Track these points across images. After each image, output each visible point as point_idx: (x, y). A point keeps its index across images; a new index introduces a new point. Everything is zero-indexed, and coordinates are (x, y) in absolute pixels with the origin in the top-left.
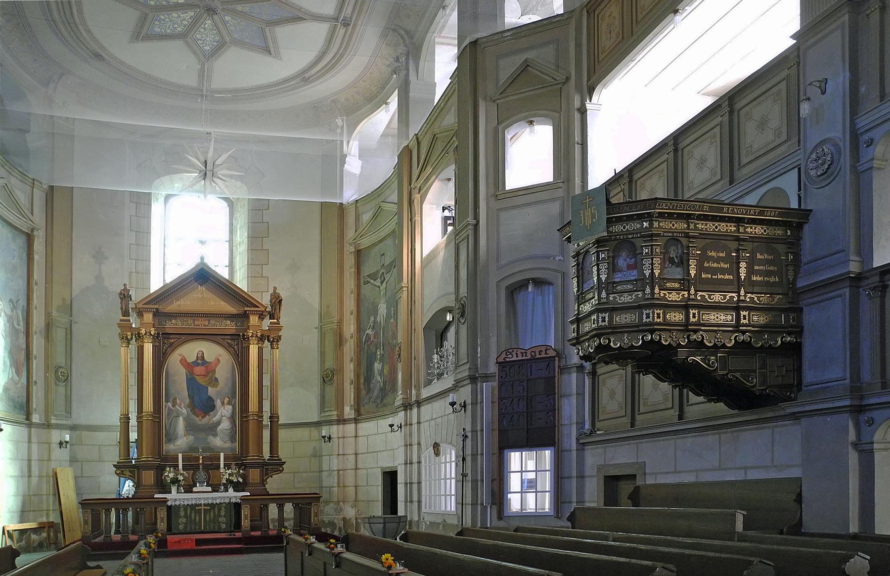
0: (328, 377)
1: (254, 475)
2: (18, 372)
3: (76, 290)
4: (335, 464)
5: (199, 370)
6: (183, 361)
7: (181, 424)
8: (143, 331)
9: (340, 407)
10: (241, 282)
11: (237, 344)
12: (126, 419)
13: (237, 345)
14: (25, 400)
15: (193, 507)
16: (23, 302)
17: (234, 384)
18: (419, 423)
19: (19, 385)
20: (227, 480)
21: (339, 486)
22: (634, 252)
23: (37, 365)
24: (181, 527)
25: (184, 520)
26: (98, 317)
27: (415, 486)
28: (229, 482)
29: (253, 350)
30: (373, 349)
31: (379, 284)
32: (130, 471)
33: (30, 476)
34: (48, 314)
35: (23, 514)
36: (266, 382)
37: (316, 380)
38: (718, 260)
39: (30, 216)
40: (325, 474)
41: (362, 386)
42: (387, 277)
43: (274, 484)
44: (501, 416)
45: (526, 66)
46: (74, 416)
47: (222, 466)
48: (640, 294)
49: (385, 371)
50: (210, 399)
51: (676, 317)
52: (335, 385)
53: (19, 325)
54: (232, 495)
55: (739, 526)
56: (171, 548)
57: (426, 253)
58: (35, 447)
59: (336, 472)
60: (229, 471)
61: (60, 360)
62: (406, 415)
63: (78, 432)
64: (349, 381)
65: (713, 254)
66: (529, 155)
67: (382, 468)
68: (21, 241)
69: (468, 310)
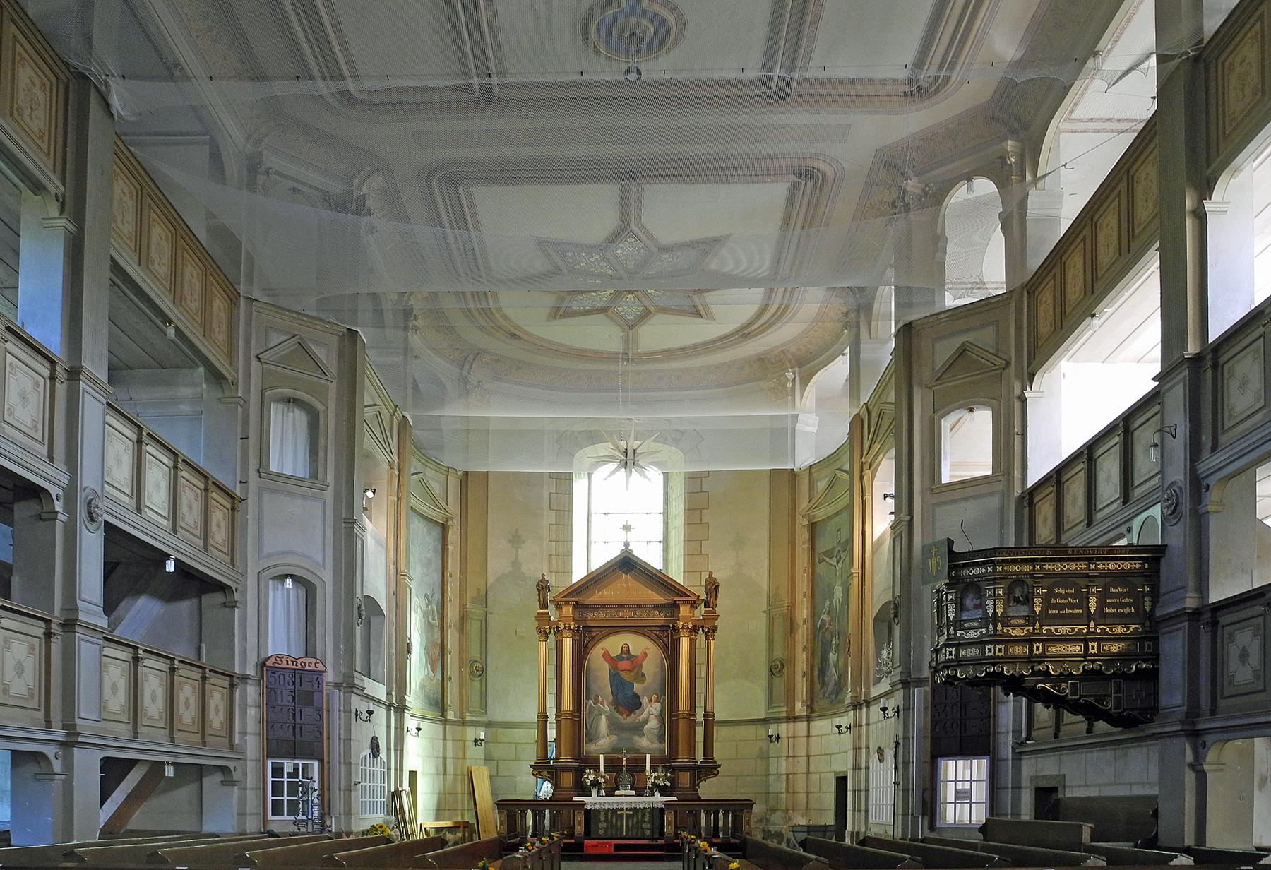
0: (777, 669)
1: (684, 778)
2: (433, 669)
5: (623, 665)
6: (606, 656)
8: (562, 626)
12: (544, 718)
13: (666, 637)
15: (614, 811)
16: (438, 596)
17: (663, 670)
18: (868, 724)
21: (787, 792)
22: (980, 594)
23: (452, 660)
24: (601, 832)
26: (514, 608)
27: (863, 794)
28: (655, 785)
29: (684, 643)
30: (827, 635)
33: (445, 774)
34: (463, 607)
37: (764, 672)
38: (1066, 596)
40: (772, 778)
43: (709, 789)
44: (934, 724)
45: (963, 351)
47: (648, 768)
48: (984, 631)
50: (637, 696)
51: (1021, 650)
54: (658, 799)
55: (1086, 836)
56: (586, 851)
57: (875, 538)
58: (449, 744)
61: (475, 653)
62: (855, 716)
65: (1061, 591)
66: (968, 446)
68: (436, 532)
69: (901, 611)
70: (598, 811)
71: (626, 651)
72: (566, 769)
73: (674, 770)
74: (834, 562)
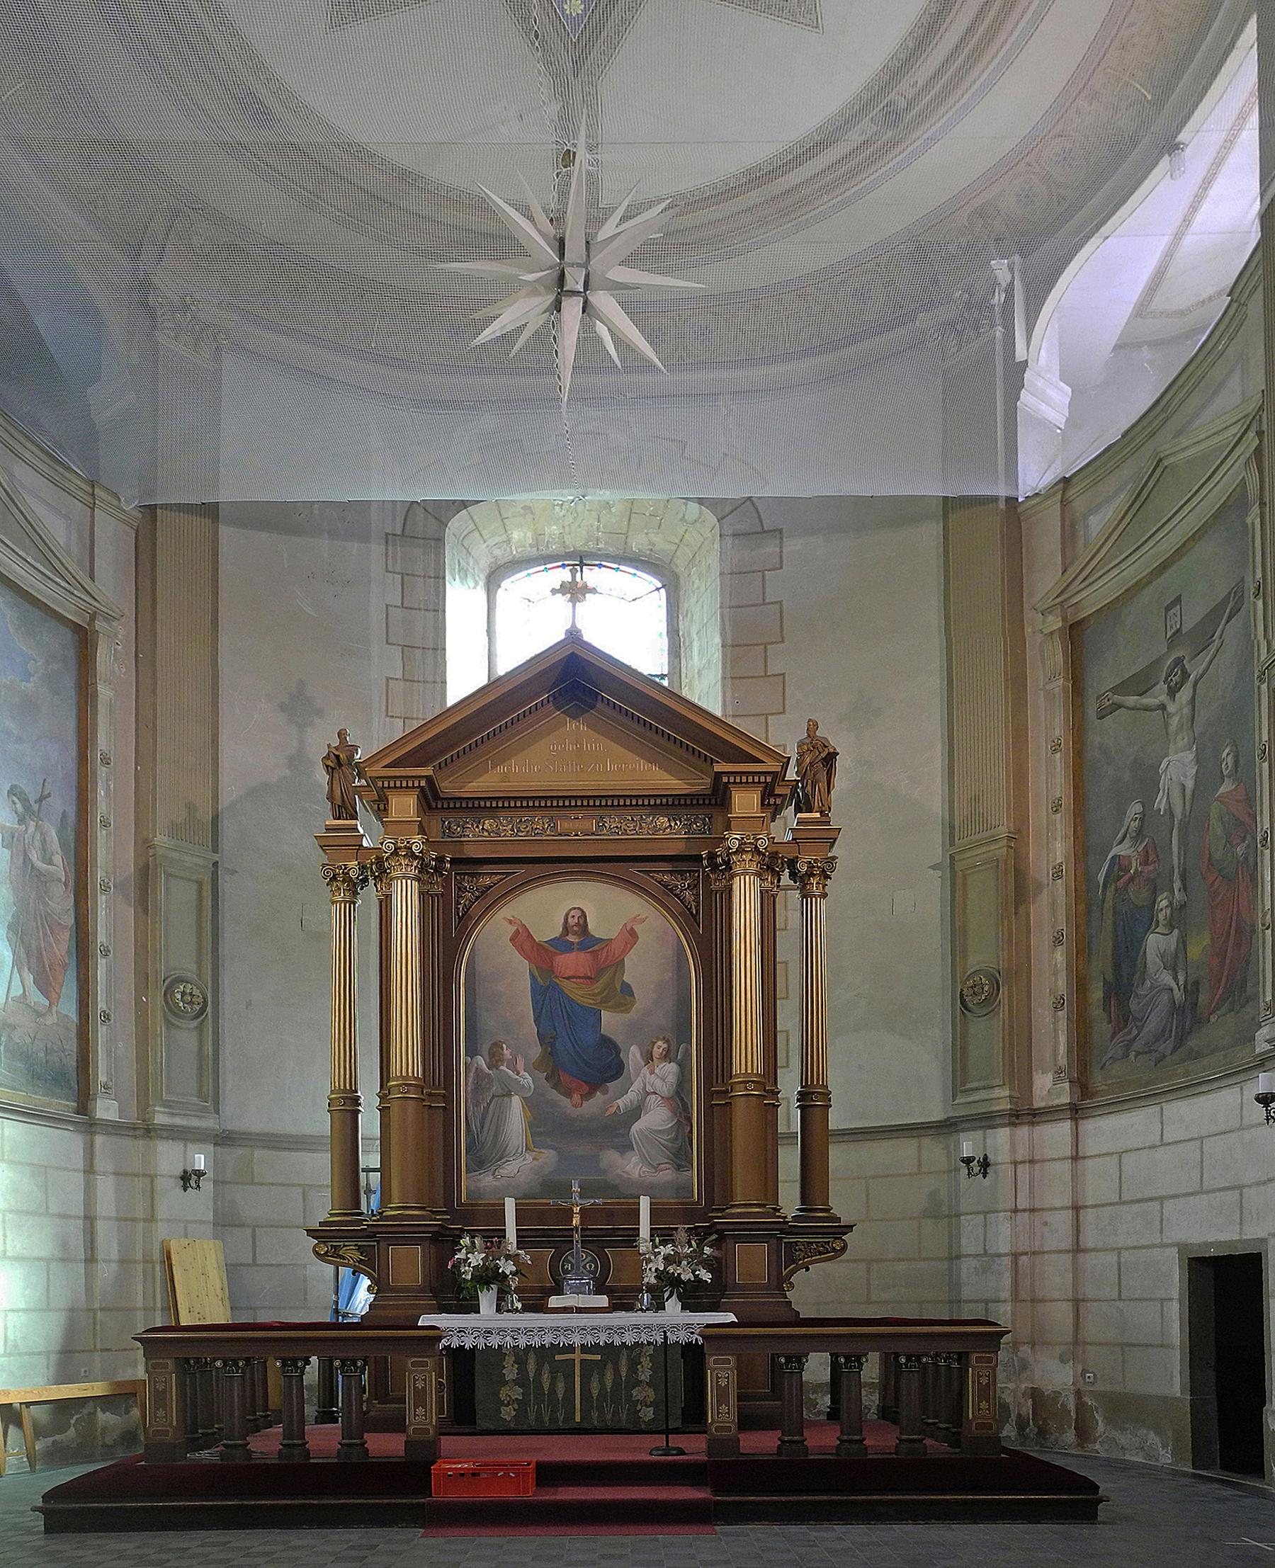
0: (974, 997)
2: (45, 984)
3: (230, 790)
4: (1004, 1236)
5: (569, 962)
6: (522, 939)
7: (516, 1117)
9: (1019, 1071)
10: (706, 690)
13: (692, 885)
14: (72, 1062)
16: (62, 803)
17: (682, 977)
19: (51, 1020)
20: (660, 1275)
21: (1016, 1298)
24: (508, 1413)
25: (517, 1393)
29: (745, 895)
31: (1163, 698)
32: (359, 1248)
33: (91, 1259)
34: (144, 844)
35: (68, 1360)
36: (788, 1019)
37: (936, 1004)
40: (967, 1266)
41: (1096, 1012)
43: (815, 1290)
46: (228, 1108)
49: (1194, 952)
50: (609, 1046)
52: (1003, 1012)
53: (50, 863)
54: (677, 1320)
58: (105, 1187)
59: (1007, 1261)
60: (668, 1250)
61: (180, 956)
63: (240, 1151)
64: (1049, 1002)
67: (1183, 1248)
68: (61, 641)
71: (578, 927)
73: (722, 1237)
74: (1159, 695)
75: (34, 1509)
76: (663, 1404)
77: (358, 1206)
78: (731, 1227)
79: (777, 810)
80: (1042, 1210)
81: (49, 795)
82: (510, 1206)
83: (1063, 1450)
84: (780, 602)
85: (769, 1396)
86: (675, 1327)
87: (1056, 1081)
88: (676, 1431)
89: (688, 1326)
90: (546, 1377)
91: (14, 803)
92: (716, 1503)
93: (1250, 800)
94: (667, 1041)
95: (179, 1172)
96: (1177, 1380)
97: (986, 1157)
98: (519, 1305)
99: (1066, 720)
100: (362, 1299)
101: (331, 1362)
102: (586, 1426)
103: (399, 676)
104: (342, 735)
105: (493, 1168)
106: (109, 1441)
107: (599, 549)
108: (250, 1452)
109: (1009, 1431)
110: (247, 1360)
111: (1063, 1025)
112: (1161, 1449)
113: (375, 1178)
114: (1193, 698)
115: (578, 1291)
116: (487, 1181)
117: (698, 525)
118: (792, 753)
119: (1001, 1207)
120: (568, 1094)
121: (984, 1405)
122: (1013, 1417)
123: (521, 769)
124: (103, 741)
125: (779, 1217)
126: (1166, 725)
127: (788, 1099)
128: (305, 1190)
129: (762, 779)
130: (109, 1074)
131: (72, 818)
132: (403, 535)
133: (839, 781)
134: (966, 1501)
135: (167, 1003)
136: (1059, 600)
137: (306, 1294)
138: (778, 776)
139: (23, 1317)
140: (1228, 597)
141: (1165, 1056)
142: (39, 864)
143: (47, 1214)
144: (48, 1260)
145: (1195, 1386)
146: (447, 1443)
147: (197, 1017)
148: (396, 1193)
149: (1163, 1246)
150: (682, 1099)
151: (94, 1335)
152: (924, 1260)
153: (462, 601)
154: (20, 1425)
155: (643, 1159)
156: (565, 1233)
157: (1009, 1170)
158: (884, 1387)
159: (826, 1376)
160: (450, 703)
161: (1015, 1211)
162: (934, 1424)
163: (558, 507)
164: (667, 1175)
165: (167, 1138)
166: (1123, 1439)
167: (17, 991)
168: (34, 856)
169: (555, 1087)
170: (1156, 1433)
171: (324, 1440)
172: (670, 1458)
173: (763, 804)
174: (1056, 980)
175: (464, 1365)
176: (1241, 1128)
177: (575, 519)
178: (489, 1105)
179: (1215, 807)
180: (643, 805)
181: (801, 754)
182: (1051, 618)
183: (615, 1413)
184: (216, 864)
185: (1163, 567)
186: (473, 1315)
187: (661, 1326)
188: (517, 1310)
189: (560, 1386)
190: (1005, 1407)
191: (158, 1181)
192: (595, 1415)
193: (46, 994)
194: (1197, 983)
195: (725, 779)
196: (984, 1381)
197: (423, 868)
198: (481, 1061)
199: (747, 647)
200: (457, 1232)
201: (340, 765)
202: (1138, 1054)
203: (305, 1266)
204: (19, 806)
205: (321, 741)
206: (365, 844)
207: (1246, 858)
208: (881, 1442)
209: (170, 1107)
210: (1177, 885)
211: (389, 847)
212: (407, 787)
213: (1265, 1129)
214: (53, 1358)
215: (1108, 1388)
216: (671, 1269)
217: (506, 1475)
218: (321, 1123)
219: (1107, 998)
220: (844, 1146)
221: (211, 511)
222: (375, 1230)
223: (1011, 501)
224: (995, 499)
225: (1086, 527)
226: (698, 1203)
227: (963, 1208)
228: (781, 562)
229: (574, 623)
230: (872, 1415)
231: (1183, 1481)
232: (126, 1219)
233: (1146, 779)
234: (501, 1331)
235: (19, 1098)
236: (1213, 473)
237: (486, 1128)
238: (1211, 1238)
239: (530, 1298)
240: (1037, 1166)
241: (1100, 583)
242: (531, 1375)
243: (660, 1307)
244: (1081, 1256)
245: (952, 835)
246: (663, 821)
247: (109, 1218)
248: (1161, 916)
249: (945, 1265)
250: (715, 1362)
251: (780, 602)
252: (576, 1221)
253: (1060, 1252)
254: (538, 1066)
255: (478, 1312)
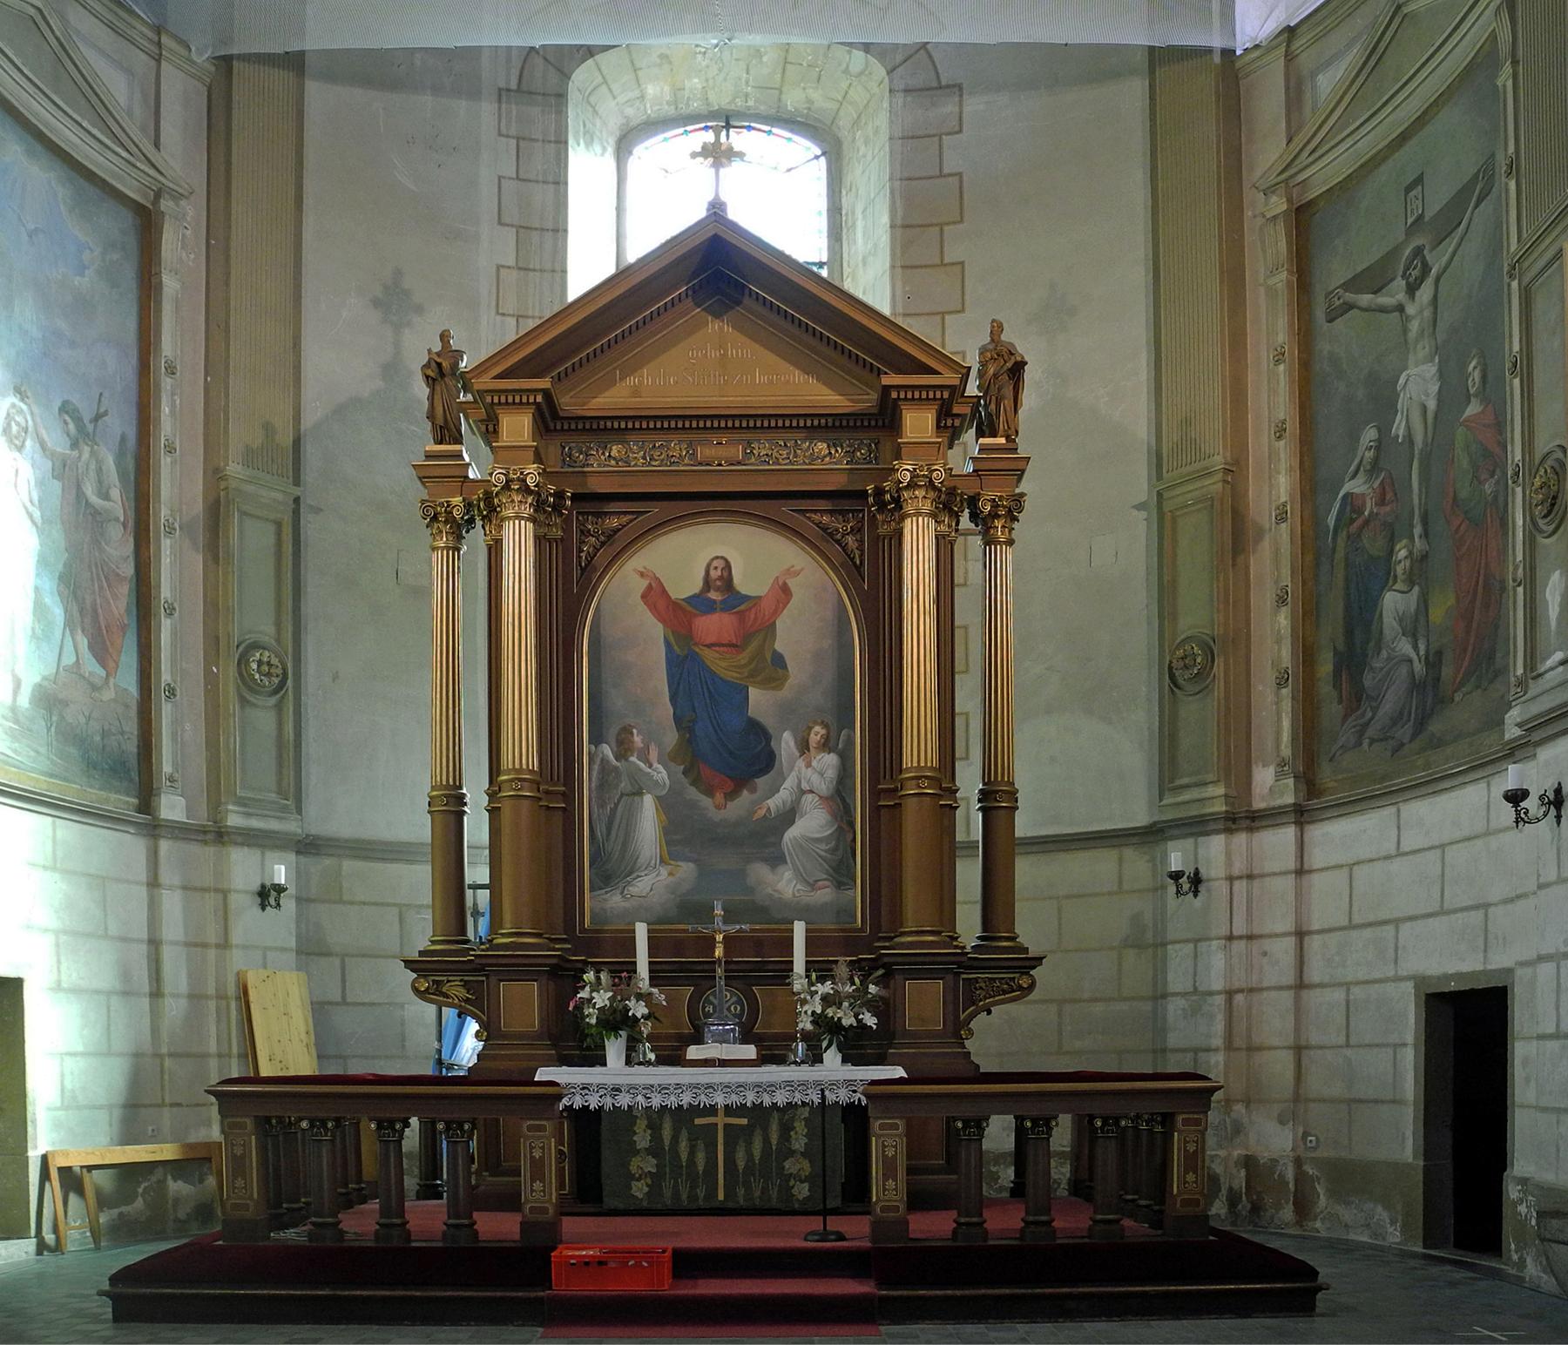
1: (924, 1001)
2: (101, 650)
4: (1217, 969)
5: (713, 626)
6: (655, 595)
9: (1238, 771)
10: (872, 283)
11: (857, 530)
13: (854, 528)
14: (132, 747)
15: (683, 1116)
16: (120, 423)
17: (844, 647)
19: (108, 695)
20: (817, 1019)
21: (1229, 1046)
24: (639, 1189)
25: (650, 1165)
29: (918, 540)
31: (1401, 296)
32: (466, 985)
34: (215, 475)
35: (134, 1115)
36: (968, 700)
39: (148, 148)
40: (1175, 1007)
41: (1325, 689)
42: (1437, 262)
43: (999, 1037)
46: (312, 808)
49: (1437, 614)
50: (758, 733)
52: (1219, 690)
53: (107, 497)
54: (836, 1074)
58: (172, 903)
59: (1220, 1000)
60: (826, 988)
61: (256, 618)
63: (328, 861)
64: (1271, 676)
67: (1420, 981)
68: (118, 224)
70: (626, 1116)
72: (513, 967)
73: (889, 971)
74: (1396, 292)
75: (101, 1293)
76: (820, 1179)
77: (463, 931)
78: (900, 959)
79: (954, 435)
80: (1261, 936)
81: (106, 413)
82: (641, 932)
83: (1279, 1231)
84: (960, 175)
85: (944, 1166)
86: (834, 1084)
87: (1279, 776)
88: (835, 1212)
89: (849, 1083)
90: (683, 1146)
91: (66, 423)
92: (882, 1299)
93: (1500, 425)
94: (825, 725)
95: (256, 886)
96: (1410, 1142)
97: (1197, 872)
98: (652, 1056)
99: (1291, 325)
100: (469, 1047)
101: (434, 1123)
102: (730, 1205)
103: (512, 262)
104: (444, 337)
105: (621, 885)
106: (182, 1215)
107: (749, 108)
108: (342, 1232)
109: (1219, 1208)
110: (337, 1120)
111: (1287, 705)
112: (1388, 1225)
113: (484, 895)
114: (1435, 298)
115: (722, 1039)
116: (614, 901)
117: (864, 78)
118: (973, 361)
119: (1213, 933)
120: (709, 792)
121: (1190, 1177)
122: (1224, 1192)
123: (654, 381)
124: (168, 346)
125: (956, 947)
126: (1405, 331)
127: (967, 799)
128: (403, 910)
129: (938, 395)
130: (175, 765)
131: (132, 442)
132: (519, 90)
133: (1029, 398)
134: (1166, 1293)
135: (240, 674)
136: (1283, 176)
137: (403, 1040)
138: (957, 391)
139: (72, 1065)
140: (1476, 175)
141: (1403, 745)
142: (94, 500)
143: (106, 936)
144: (109, 993)
145: (1429, 1149)
146: (569, 1225)
147: (275, 692)
148: (507, 916)
149: (1398, 979)
150: (843, 800)
151: (163, 1087)
152: (1125, 999)
153: (587, 169)
154: (80, 1192)
155: (799, 876)
156: (706, 967)
157: (1223, 887)
158: (1076, 1157)
159: (1009, 1143)
160: (572, 296)
161: (1230, 938)
162: (1133, 1201)
163: (702, 58)
164: (825, 894)
165: (242, 844)
166: (1347, 1214)
167: (69, 659)
168: (89, 491)
169: (693, 783)
170: (1386, 1208)
171: (427, 1219)
172: (828, 1244)
173: (938, 427)
174: (1279, 650)
175: (589, 1129)
176: (1488, 833)
177: (720, 70)
178: (616, 805)
179: (1460, 431)
180: (798, 427)
181: (983, 364)
182: (1274, 199)
183: (764, 1190)
184: (297, 500)
185: (1403, 138)
186: (598, 1069)
187: (817, 1083)
188: (649, 1063)
189: (701, 1158)
190: (1214, 1180)
191: (233, 897)
192: (741, 1192)
193: (102, 662)
194: (1439, 653)
195: (894, 395)
196: (1191, 1148)
197: (539, 506)
198: (607, 750)
199: (922, 225)
200: (580, 965)
201: (442, 374)
202: (1372, 741)
203: (402, 1006)
204: (71, 426)
205: (419, 347)
206: (471, 476)
207: (1496, 498)
208: (1072, 1223)
209: (245, 805)
210: (1418, 530)
211: (498, 478)
212: (521, 403)
213: (1512, 836)
214: (117, 1113)
215: (1332, 1154)
216: (830, 1012)
217: (638, 1265)
218: (419, 827)
219: (1337, 672)
220: (1032, 858)
221: (295, 63)
222: (484, 961)
223: (1228, 53)
224: (1209, 51)
225: (1314, 87)
226: (862, 930)
227: (1170, 937)
228: (961, 125)
229: (717, 194)
230: (1062, 1191)
231: (1413, 1263)
232: (196, 945)
233: (1382, 399)
234: (632, 1088)
235: (73, 791)
236: (1379, 110)
237: (613, 833)
238: (1451, 968)
239: (664, 1048)
240: (1256, 883)
241: (1330, 157)
242: (667, 1143)
243: (816, 1058)
244: (1304, 993)
245: (1159, 466)
246: (822, 447)
247: (176, 943)
248: (1399, 569)
249: (1147, 1007)
250: (882, 1127)
251: (960, 175)
252: (719, 952)
253: (1281, 988)
254: (669, 759)
255: (604, 1064)
